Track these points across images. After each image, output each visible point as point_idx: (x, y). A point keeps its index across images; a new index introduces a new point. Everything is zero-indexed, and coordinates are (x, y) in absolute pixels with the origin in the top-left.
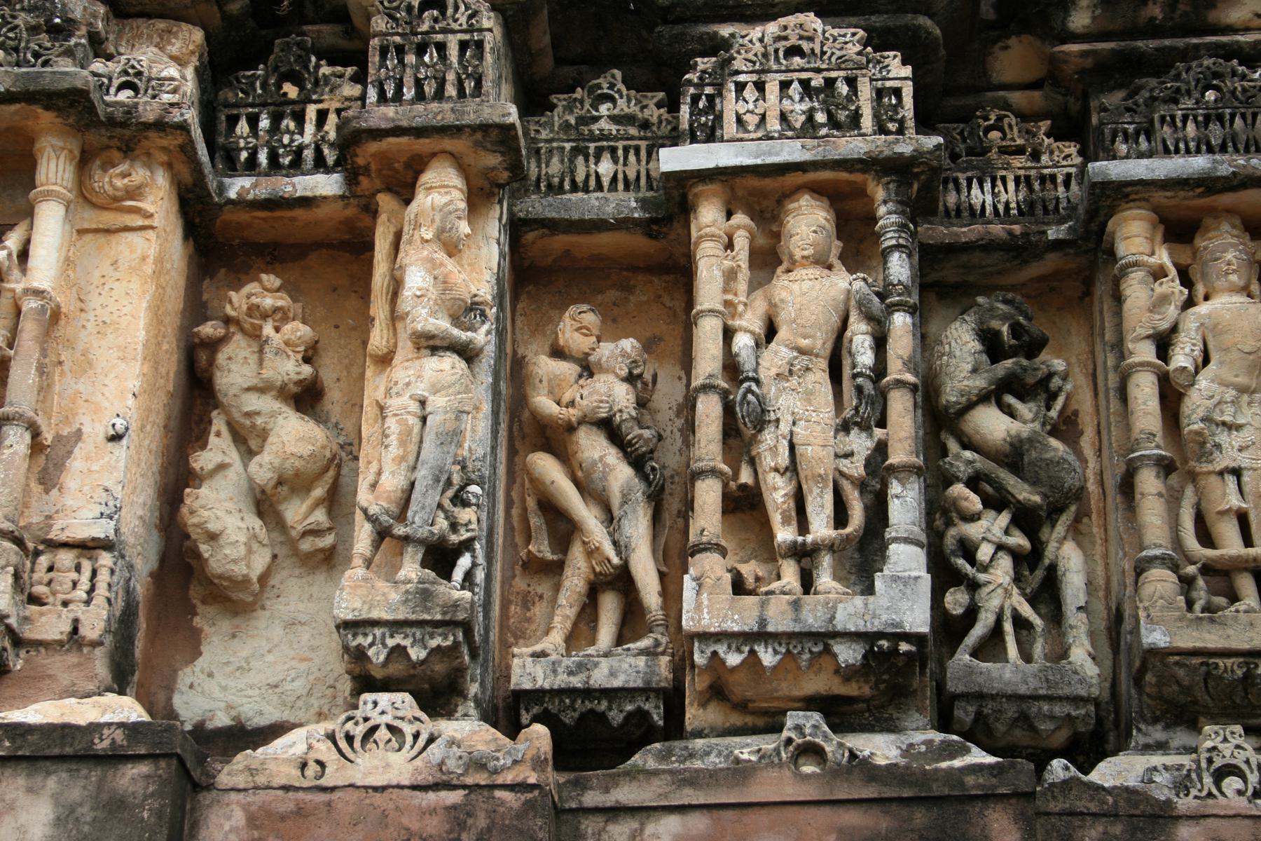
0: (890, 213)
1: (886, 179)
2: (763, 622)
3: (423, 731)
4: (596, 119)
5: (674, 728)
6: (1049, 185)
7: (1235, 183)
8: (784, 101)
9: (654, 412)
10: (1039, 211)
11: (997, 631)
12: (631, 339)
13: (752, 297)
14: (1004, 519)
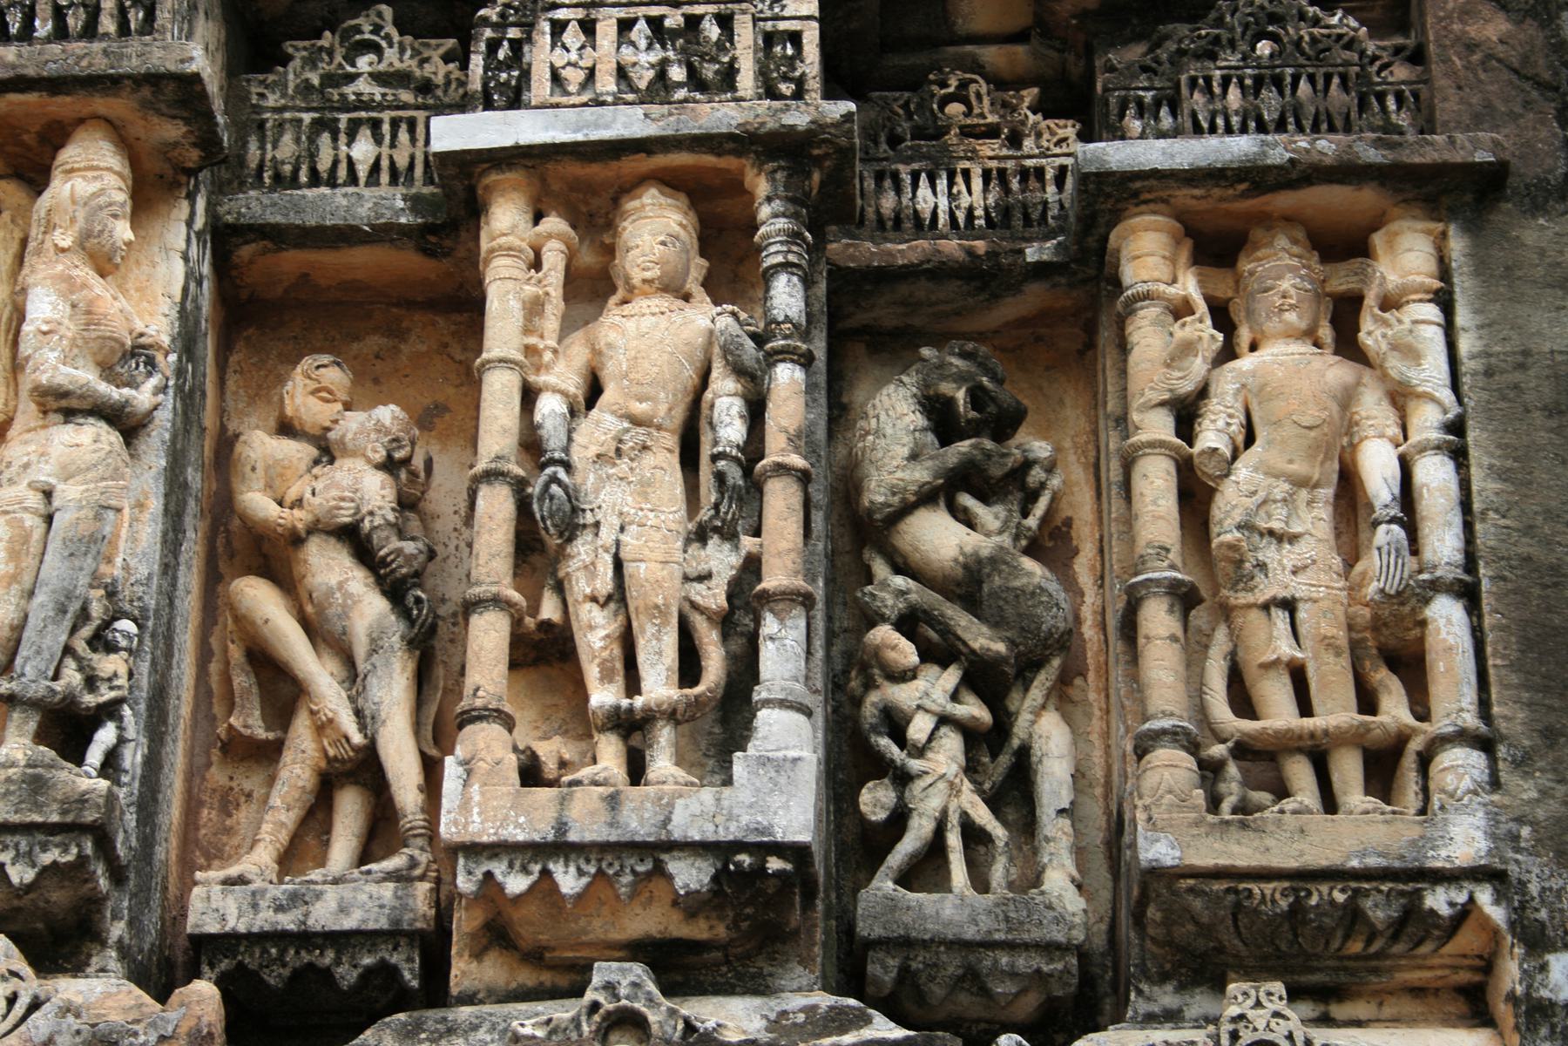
0: (775, 216)
1: (771, 166)
2: (561, 827)
3: (22, 993)
4: (352, 78)
5: (435, 991)
6: (1033, 183)
7: (1294, 176)
8: (624, 49)
9: (426, 520)
10: (1017, 222)
11: (936, 848)
12: (392, 407)
13: (567, 341)
14: (952, 677)
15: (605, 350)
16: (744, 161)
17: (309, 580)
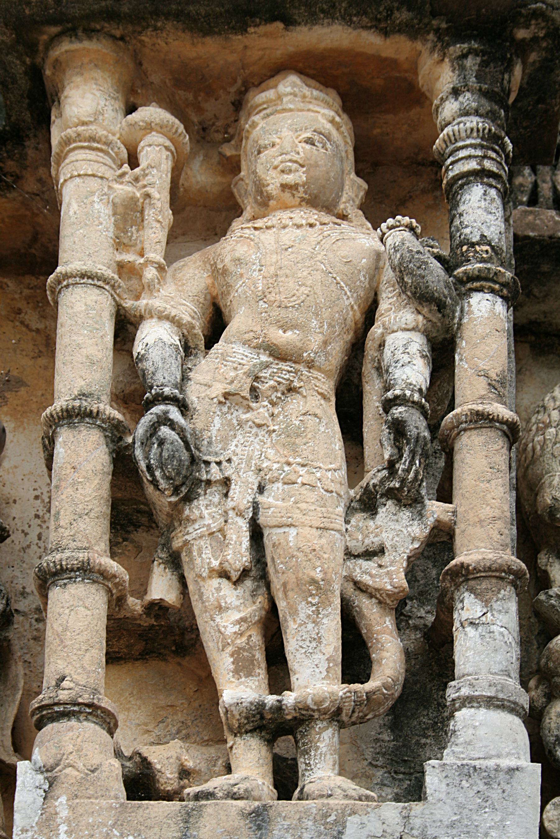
1: (457, 49)
15: (231, 268)
16: (419, 45)
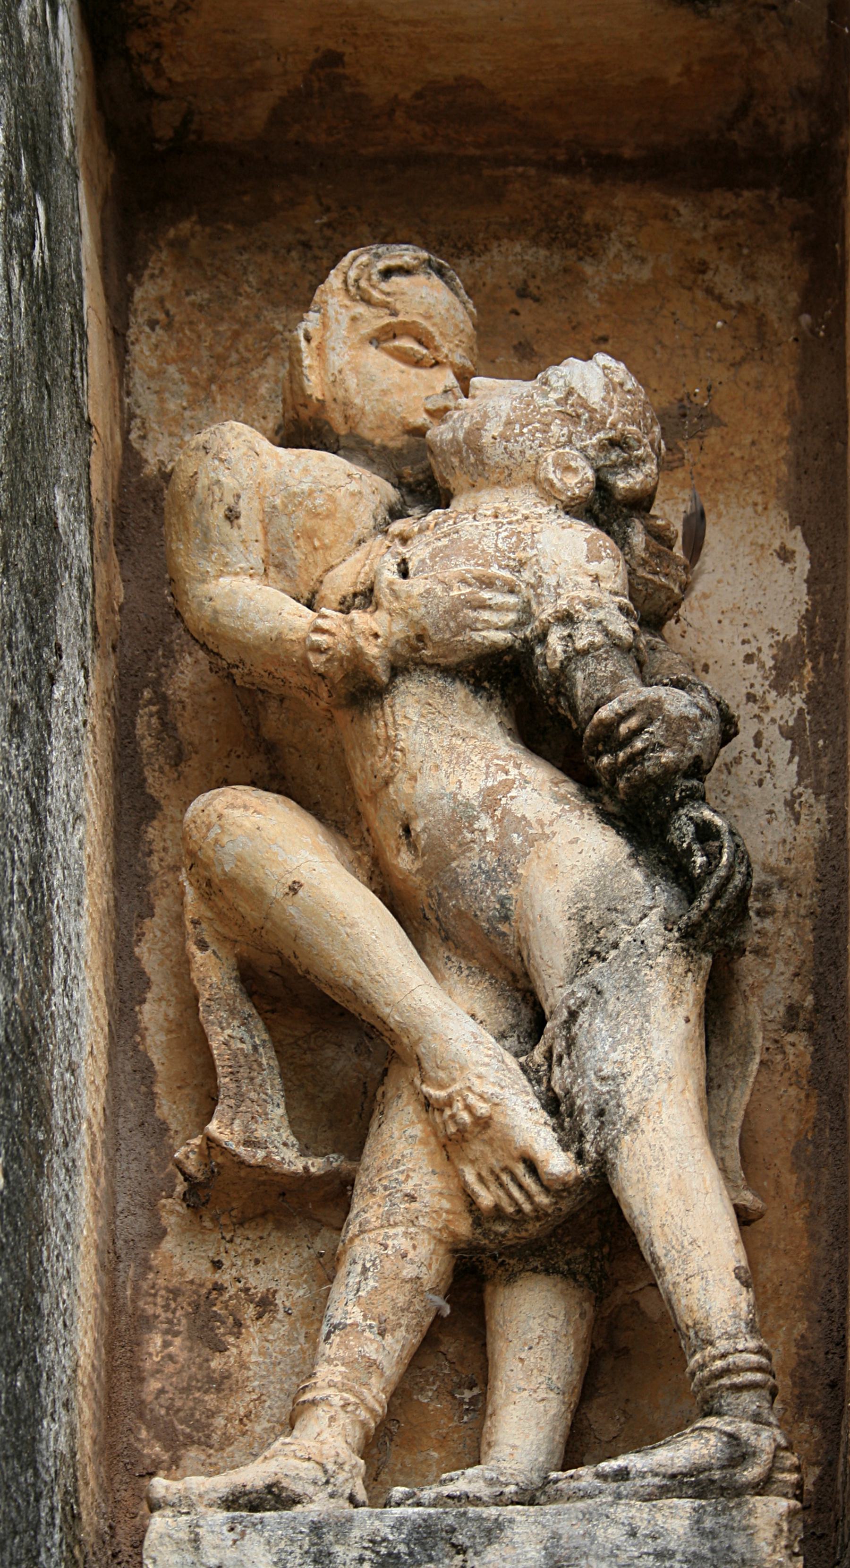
17: (402, 786)
